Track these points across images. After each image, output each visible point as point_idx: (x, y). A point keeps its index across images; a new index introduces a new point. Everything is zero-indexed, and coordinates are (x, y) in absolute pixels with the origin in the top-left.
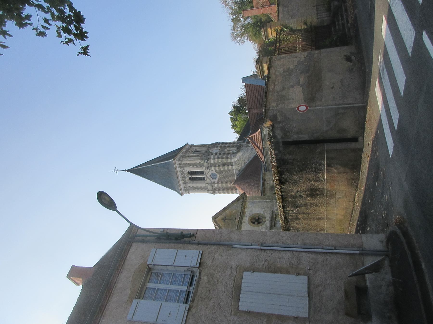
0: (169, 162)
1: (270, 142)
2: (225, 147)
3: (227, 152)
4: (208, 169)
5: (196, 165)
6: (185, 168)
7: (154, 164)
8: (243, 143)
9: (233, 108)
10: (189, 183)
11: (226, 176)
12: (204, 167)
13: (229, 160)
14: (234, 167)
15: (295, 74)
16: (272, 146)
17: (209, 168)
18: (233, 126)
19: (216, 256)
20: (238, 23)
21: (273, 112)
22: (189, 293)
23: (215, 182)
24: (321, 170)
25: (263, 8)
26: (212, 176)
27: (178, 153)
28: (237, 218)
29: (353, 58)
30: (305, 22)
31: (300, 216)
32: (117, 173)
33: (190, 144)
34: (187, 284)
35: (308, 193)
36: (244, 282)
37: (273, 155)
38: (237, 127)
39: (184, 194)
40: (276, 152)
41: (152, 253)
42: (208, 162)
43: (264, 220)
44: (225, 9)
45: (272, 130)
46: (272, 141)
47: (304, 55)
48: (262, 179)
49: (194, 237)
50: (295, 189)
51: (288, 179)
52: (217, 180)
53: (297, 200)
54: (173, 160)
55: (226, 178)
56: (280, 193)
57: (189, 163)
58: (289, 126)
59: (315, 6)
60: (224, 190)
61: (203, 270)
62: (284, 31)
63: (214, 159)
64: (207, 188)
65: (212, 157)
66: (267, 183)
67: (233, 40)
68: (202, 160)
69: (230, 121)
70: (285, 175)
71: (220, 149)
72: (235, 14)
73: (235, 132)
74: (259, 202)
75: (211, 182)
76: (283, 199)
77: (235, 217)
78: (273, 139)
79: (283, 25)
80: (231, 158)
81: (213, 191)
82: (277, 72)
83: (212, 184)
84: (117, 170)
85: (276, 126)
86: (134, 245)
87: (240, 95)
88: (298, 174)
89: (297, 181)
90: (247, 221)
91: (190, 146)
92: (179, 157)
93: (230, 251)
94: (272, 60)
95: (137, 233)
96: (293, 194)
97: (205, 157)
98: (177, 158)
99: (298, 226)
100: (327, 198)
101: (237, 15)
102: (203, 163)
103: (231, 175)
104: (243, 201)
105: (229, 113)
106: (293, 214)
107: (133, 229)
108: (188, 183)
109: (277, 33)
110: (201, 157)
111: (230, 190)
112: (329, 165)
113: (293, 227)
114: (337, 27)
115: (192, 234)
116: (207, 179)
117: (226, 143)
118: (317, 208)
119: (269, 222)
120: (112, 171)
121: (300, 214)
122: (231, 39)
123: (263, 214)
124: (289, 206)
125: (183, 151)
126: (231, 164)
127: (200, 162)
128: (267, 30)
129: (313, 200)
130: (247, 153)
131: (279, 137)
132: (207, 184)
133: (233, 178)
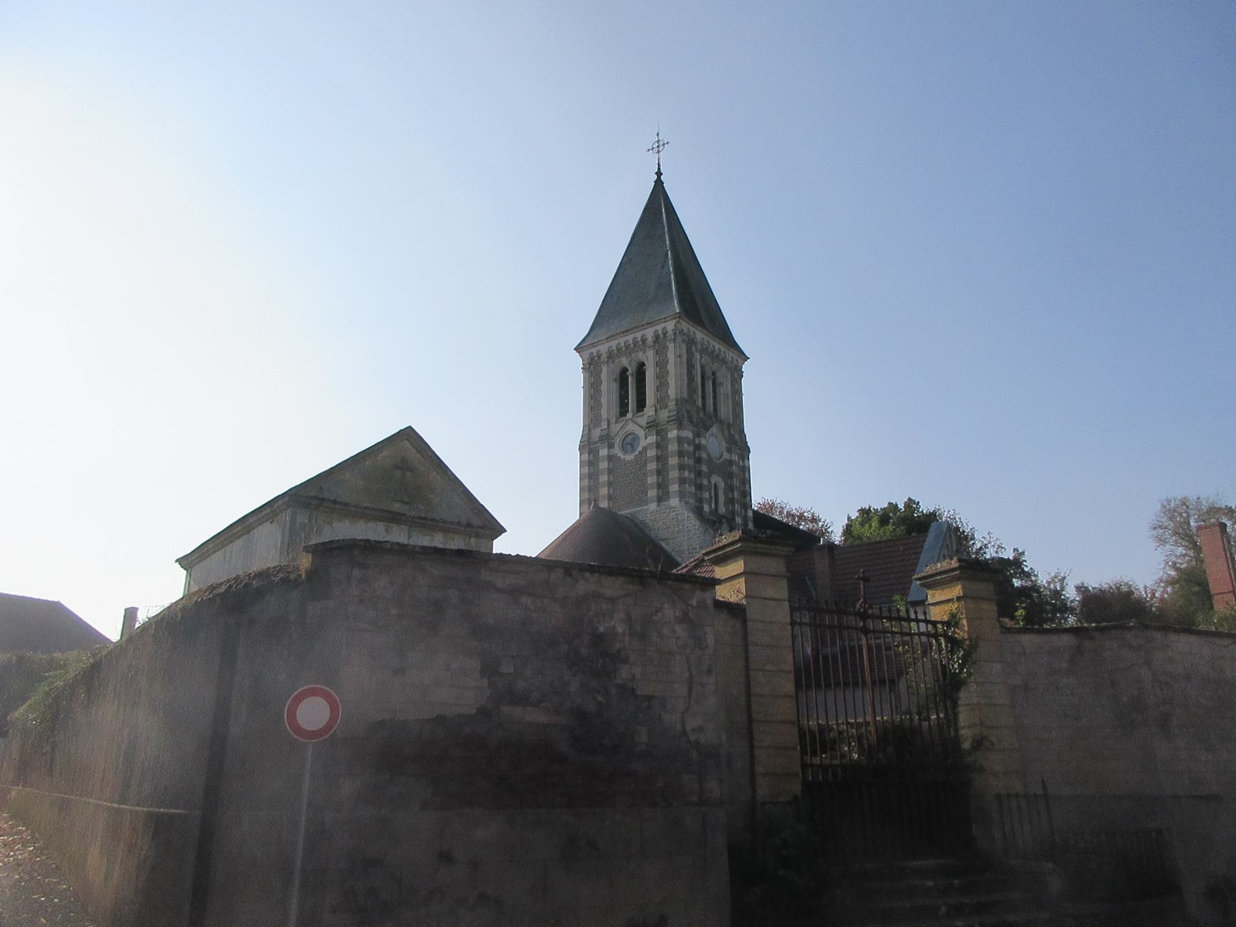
2: (729, 476)
3: (705, 482)
4: (648, 425)
5: (662, 385)
12: (656, 411)
13: (674, 488)
14: (653, 506)
17: (653, 426)
18: (865, 513)
27: (707, 330)
28: (407, 507)
39: (581, 356)
42: (668, 422)
52: (618, 455)
59: (1044, 788)
62: (952, 652)
63: (680, 440)
64: (595, 427)
65: (688, 434)
71: (721, 460)
75: (612, 435)
80: (682, 495)
83: (607, 439)
98: (685, 325)
102: (666, 407)
104: (469, 525)
110: (690, 400)
116: (621, 425)
120: (658, 135)
128: (954, 583)
132: (608, 425)
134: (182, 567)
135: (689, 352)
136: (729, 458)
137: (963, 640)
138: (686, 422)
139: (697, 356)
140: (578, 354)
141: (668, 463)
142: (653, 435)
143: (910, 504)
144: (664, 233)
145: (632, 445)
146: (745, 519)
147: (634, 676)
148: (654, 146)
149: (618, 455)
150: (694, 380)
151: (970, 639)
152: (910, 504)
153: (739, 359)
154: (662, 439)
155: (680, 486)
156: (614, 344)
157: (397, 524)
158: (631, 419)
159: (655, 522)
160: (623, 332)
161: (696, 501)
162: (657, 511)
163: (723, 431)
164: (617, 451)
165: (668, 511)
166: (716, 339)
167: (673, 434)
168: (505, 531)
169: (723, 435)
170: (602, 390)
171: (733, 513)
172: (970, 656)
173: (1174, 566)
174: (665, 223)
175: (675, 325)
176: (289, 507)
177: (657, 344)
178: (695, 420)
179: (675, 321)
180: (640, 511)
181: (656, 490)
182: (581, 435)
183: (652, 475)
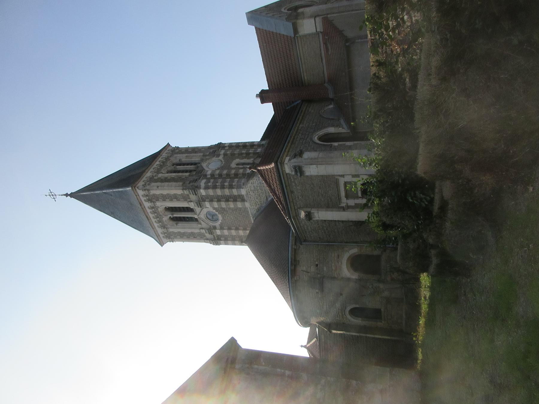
4: (199, 207)
5: (175, 197)
6: (157, 203)
12: (191, 201)
13: (235, 192)
14: (247, 204)
17: (200, 203)
32: (54, 198)
33: (173, 145)
48: (291, 262)
52: (220, 223)
55: (234, 221)
57: (162, 194)
63: (207, 188)
66: (303, 271)
71: (223, 161)
75: (208, 227)
80: (239, 187)
81: (214, 242)
83: (211, 230)
98: (141, 184)
102: (188, 195)
103: (244, 216)
108: (169, 226)
116: (202, 222)
125: (155, 166)
127: (183, 193)
133: (247, 221)
135: (156, 181)
138: (196, 184)
139: (160, 175)
140: (165, 245)
142: (205, 203)
144: (95, 194)
145: (213, 216)
148: (53, 197)
149: (220, 223)
153: (168, 149)
154: (208, 198)
158: (198, 216)
161: (244, 178)
162: (250, 202)
163: (207, 159)
164: (217, 224)
165: (249, 196)
166: (153, 164)
167: (203, 192)
169: (209, 159)
175: (140, 190)
177: (153, 200)
178: (197, 178)
179: (137, 189)
181: (238, 203)
183: (229, 204)
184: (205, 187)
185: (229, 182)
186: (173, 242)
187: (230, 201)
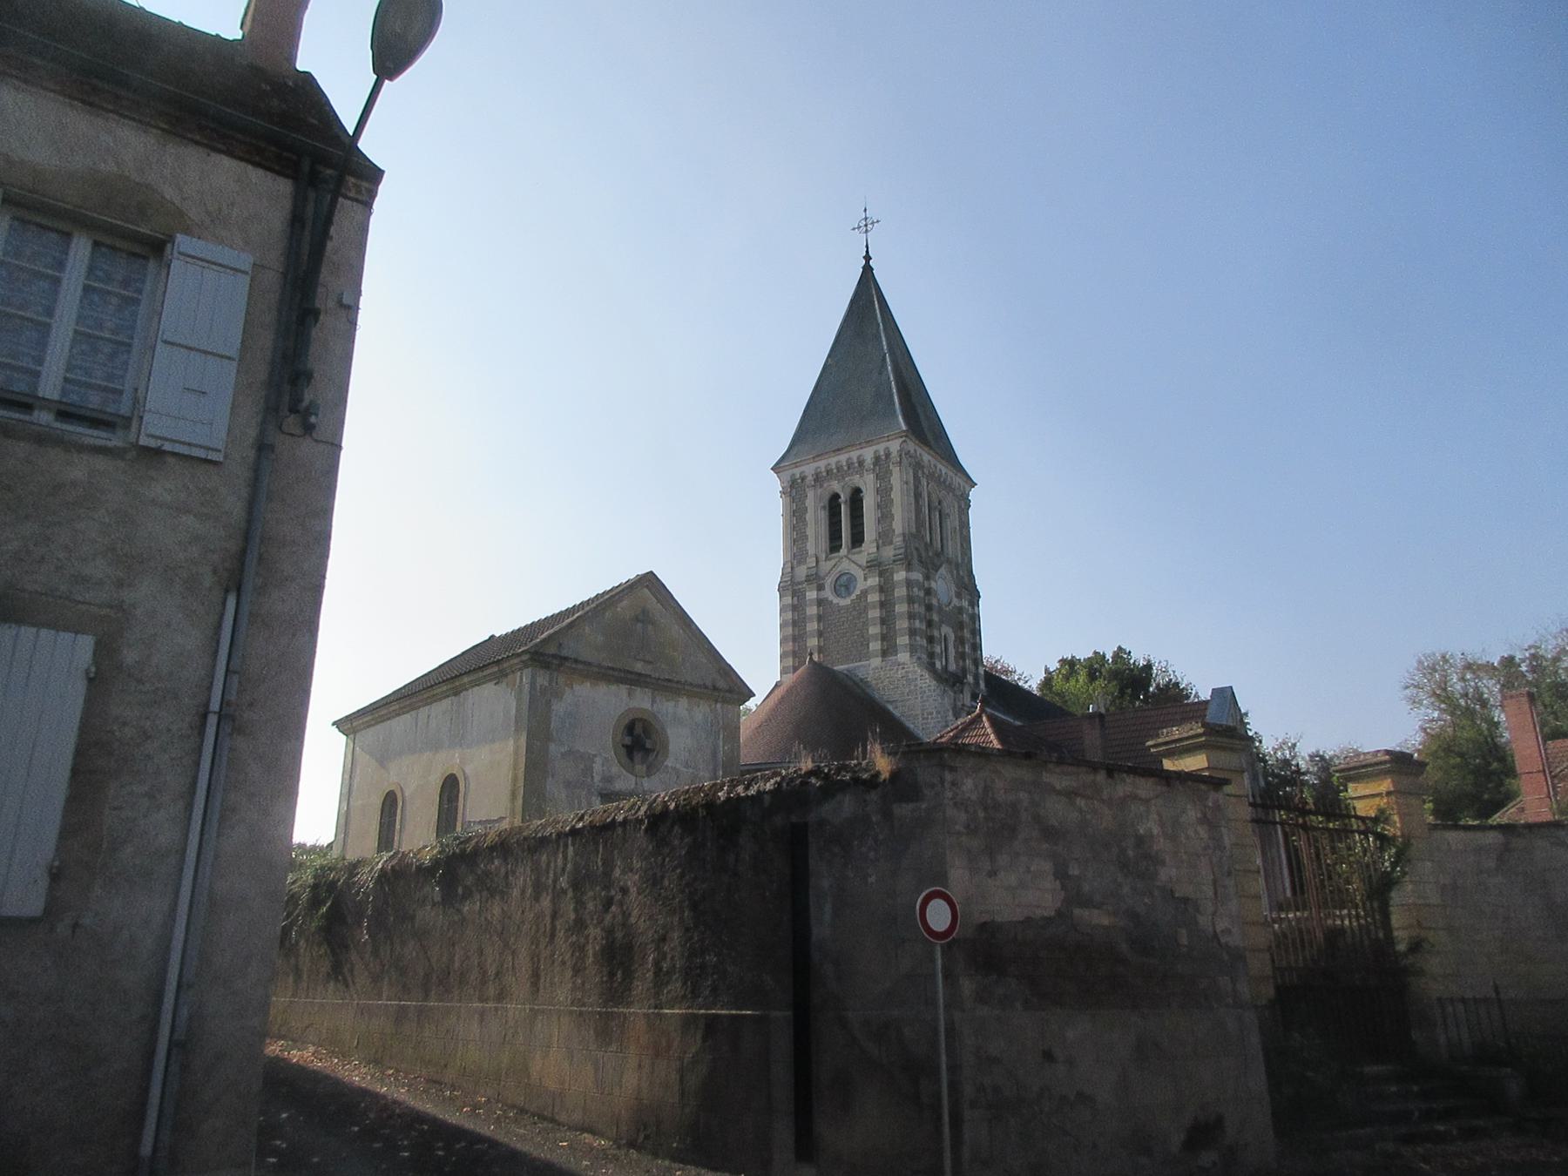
0: (897, 417)
1: (810, 773)
2: (960, 626)
3: (936, 633)
4: (869, 564)
5: (885, 516)
7: (888, 360)
8: (969, 696)
9: (1142, 663)
10: (819, 494)
11: (847, 632)
13: (903, 640)
14: (876, 662)
15: (1126, 890)
16: (792, 780)
17: (875, 565)
18: (1070, 665)
19: (189, 520)
20: (1495, 684)
21: (933, 786)
22: (27, 407)
23: (824, 589)
24: (695, 993)
25: (1543, 778)
26: (845, 578)
28: (650, 667)
29: (1208, 1158)
30: (1423, 944)
31: (546, 902)
34: (74, 398)
35: (619, 935)
36: (37, 636)
37: (756, 787)
38: (1067, 678)
40: (767, 798)
41: (226, 255)
42: (894, 561)
43: (640, 768)
44: (1554, 629)
45: (856, 781)
46: (813, 780)
47: (1228, 931)
49: (298, 431)
50: (632, 880)
51: (666, 850)
53: (598, 888)
54: (904, 428)
56: (620, 818)
57: (891, 489)
58: (872, 854)
59: (1497, 993)
60: (793, 627)
61: (121, 464)
62: (1382, 849)
63: (909, 584)
64: (799, 563)
65: (917, 576)
67: (1420, 662)
68: (904, 537)
69: (1090, 655)
70: (682, 839)
71: (950, 607)
72: (1533, 669)
73: (1047, 670)
74: (714, 754)
75: (822, 575)
76: (603, 830)
77: (651, 659)
78: (821, 786)
79: (1407, 843)
80: (913, 649)
82: (1142, 808)
83: (815, 580)
84: (870, 226)
85: (873, 796)
86: (284, 186)
87: (1194, 692)
88: (683, 892)
89: (660, 889)
90: (637, 706)
91: (962, 495)
92: (915, 451)
93: (208, 581)
94: (1203, 787)
95: (346, 197)
96: (617, 873)
97: (917, 549)
98: (912, 446)
99: (516, 892)
100: (599, 1013)
101: (1530, 677)
102: (891, 543)
104: (715, 688)
105: (1120, 648)
106: (555, 874)
107: (359, 182)
108: (819, 491)
109: (1370, 818)
111: (794, 646)
112: (712, 1024)
113: (514, 872)
114: (1393, 1089)
115: (313, 419)
116: (833, 562)
117: (976, 632)
118: (569, 973)
119: (632, 787)
120: (865, 210)
121: (553, 901)
122: (1424, 655)
123: (667, 766)
124: (578, 857)
125: (939, 466)
126: (888, 649)
127: (896, 532)
129: (595, 955)
130: (930, 710)
131: (826, 810)
132: (817, 562)
134: (340, 731)
136: (958, 605)
137: (1395, 836)
141: (894, 611)
143: (1120, 653)
145: (847, 587)
146: (976, 677)
147: (1171, 878)
150: (921, 511)
151: (1403, 836)
152: (1120, 653)
155: (910, 638)
156: (822, 464)
157: (641, 687)
159: (880, 681)
160: (834, 451)
162: (882, 668)
163: (951, 572)
164: (828, 594)
168: (754, 695)
169: (952, 576)
170: (807, 519)
171: (964, 671)
172: (1403, 854)
173: (1424, 730)
174: (880, 320)
176: (526, 666)
179: (901, 440)
180: (858, 667)
182: (781, 574)
184: (910, 580)
185: (920, 629)
186: (783, 493)
187: (882, 628)
